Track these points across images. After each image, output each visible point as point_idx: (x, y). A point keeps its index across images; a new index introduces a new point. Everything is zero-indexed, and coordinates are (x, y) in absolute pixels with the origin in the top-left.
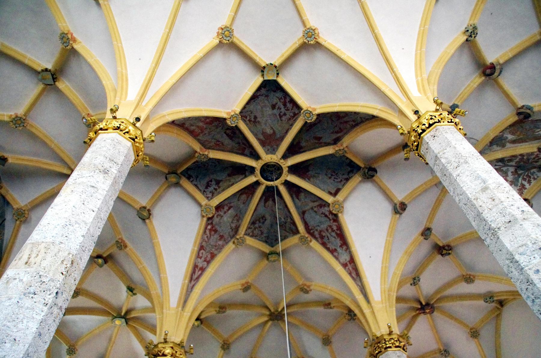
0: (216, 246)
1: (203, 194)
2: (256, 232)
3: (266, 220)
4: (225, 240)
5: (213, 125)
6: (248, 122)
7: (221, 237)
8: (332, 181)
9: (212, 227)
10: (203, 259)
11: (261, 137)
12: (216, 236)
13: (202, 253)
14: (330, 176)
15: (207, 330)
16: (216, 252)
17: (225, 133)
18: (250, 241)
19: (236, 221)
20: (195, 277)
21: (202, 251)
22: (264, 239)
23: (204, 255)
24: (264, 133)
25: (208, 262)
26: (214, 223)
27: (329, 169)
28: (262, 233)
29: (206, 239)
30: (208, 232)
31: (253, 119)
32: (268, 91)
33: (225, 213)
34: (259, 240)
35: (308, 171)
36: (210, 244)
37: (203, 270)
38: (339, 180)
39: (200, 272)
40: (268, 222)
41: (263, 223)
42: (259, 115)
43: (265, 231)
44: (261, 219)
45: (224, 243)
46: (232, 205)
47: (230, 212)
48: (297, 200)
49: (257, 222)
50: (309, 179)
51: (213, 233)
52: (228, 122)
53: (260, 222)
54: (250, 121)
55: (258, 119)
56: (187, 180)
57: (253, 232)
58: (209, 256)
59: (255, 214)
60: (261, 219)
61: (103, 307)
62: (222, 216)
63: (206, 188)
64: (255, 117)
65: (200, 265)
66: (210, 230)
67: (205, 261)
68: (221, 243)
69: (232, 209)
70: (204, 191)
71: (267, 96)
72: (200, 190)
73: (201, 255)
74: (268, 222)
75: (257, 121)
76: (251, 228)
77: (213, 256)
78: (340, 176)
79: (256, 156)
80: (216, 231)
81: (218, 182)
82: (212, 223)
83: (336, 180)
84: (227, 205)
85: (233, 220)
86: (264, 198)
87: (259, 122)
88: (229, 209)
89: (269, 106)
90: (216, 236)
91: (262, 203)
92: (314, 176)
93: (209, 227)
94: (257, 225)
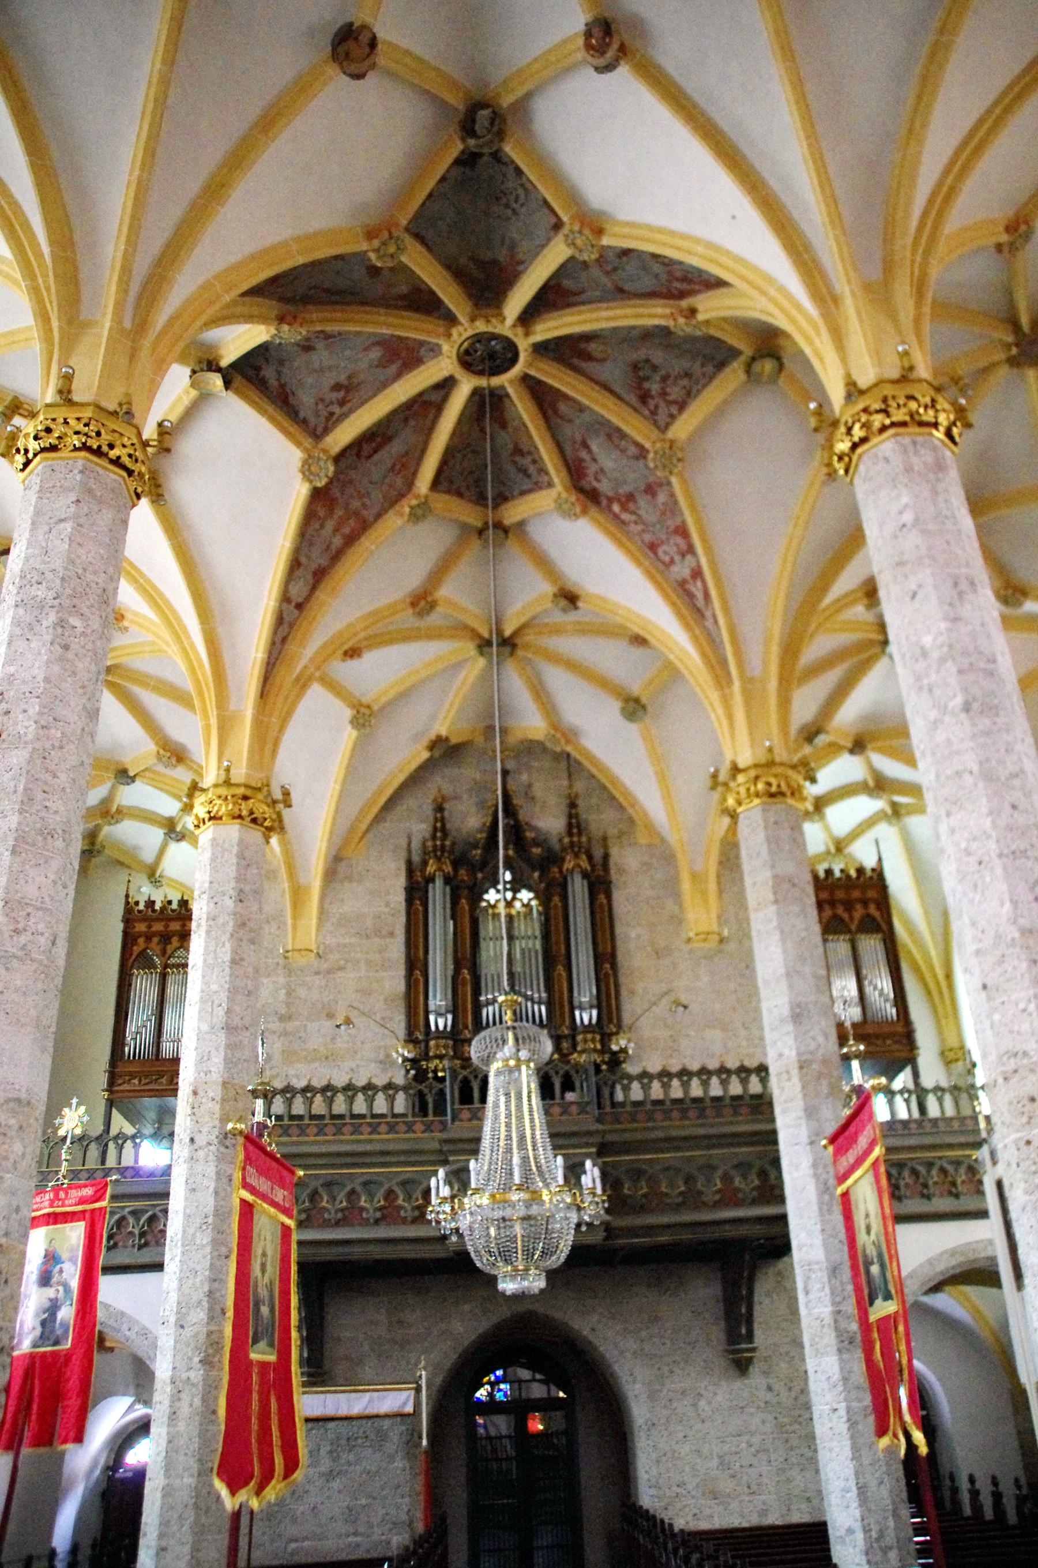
0: (663, 513)
1: (541, 488)
2: (675, 392)
3: (647, 361)
4: (661, 485)
5: (338, 495)
6: (345, 409)
7: (650, 490)
8: (523, 210)
9: (619, 500)
10: (677, 558)
11: (393, 368)
12: (643, 501)
13: (665, 552)
14: (509, 212)
15: (992, 515)
16: (678, 521)
17: (369, 457)
18: (682, 428)
19: (623, 443)
20: (700, 602)
21: (660, 551)
22: (710, 369)
23: (673, 550)
24: (382, 364)
25: (691, 550)
26: (610, 494)
27: (487, 214)
28: (687, 375)
29: (640, 527)
30: (625, 516)
31: (342, 394)
32: (267, 360)
33: (595, 460)
34: (705, 386)
35: (494, 262)
36: (654, 525)
37: (697, 573)
38: (520, 191)
39: (699, 583)
40: (658, 356)
41: (655, 368)
42: (328, 380)
43: (685, 364)
44: (641, 374)
45: (665, 488)
46: (578, 438)
47: (594, 447)
48: (584, 297)
49: (646, 385)
50: (521, 262)
51: (631, 506)
52: (320, 484)
53: (647, 379)
54: (342, 403)
55: (342, 378)
56: (510, 504)
57: (670, 403)
58: (679, 540)
59: (617, 389)
60: (641, 374)
61: (855, 659)
62: (602, 470)
63: (529, 476)
64: (337, 387)
65: (686, 573)
66: (624, 508)
67: (683, 556)
68: (662, 497)
69: (589, 442)
70: (536, 483)
71: (281, 362)
72: (530, 491)
73: (667, 559)
74: (658, 356)
75: (346, 383)
76: (657, 407)
77: (682, 531)
78: (510, 185)
79: (447, 385)
80: (631, 497)
81: (518, 451)
82: (610, 500)
83: (522, 199)
84: (577, 450)
85: (617, 447)
86: (575, 361)
87: (349, 377)
88: (585, 445)
89: (305, 357)
90: (643, 501)
91: (589, 366)
92: (512, 247)
93: (616, 508)
94: (655, 387)
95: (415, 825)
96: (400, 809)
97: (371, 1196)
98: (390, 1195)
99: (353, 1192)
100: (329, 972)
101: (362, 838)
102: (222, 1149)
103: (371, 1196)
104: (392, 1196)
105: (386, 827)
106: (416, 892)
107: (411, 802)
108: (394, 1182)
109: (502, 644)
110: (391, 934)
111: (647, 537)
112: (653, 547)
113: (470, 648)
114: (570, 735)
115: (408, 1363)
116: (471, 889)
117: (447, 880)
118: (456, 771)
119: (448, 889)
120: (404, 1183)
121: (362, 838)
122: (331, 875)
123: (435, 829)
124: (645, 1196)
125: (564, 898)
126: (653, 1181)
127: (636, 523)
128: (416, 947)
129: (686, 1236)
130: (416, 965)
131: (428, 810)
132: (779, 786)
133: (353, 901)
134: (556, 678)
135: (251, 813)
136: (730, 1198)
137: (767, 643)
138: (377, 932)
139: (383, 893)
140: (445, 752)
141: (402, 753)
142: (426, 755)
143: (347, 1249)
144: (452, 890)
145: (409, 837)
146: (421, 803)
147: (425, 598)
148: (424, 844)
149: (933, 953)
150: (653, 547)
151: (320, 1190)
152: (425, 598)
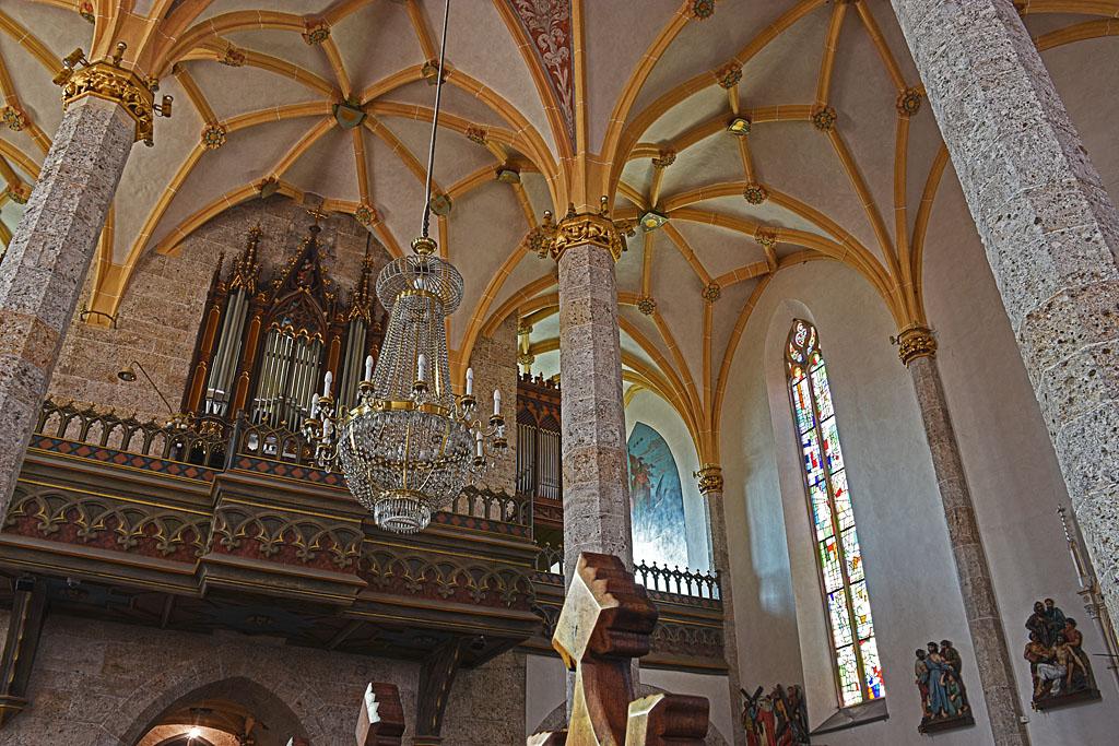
20: (562, 87)
21: (540, 39)
25: (568, 43)
58: (559, 33)
73: (544, 46)
77: (566, 27)
95: (229, 245)
96: (223, 229)
97: (131, 524)
98: (150, 527)
99: (113, 516)
100: (120, 342)
101: (175, 246)
102: (17, 383)
103: (131, 524)
104: (152, 529)
105: (204, 241)
106: (218, 297)
107: (228, 228)
108: (156, 516)
109: (353, 110)
110: (186, 327)
111: (533, 25)
112: (535, 34)
113: (328, 101)
114: (379, 216)
115: (116, 705)
116: (266, 310)
117: (248, 296)
118: (273, 218)
119: (247, 302)
120: (165, 519)
121: (175, 246)
122: (141, 264)
123: (248, 253)
124: (389, 577)
125: (344, 340)
126: (398, 566)
127: (527, 9)
128: (208, 341)
129: (419, 620)
130: (203, 355)
131: (244, 239)
132: (606, 234)
133: (155, 289)
134: (384, 160)
135: (132, 98)
136: (461, 594)
137: (609, 134)
138: (174, 321)
139: (184, 291)
140: (271, 198)
141: (235, 183)
142: (256, 192)
143: (94, 568)
144: (250, 304)
145: (222, 255)
146: (241, 231)
147: (321, 24)
148: (235, 261)
149: (698, 379)
150: (535, 34)
151: (79, 509)
152: (321, 24)
